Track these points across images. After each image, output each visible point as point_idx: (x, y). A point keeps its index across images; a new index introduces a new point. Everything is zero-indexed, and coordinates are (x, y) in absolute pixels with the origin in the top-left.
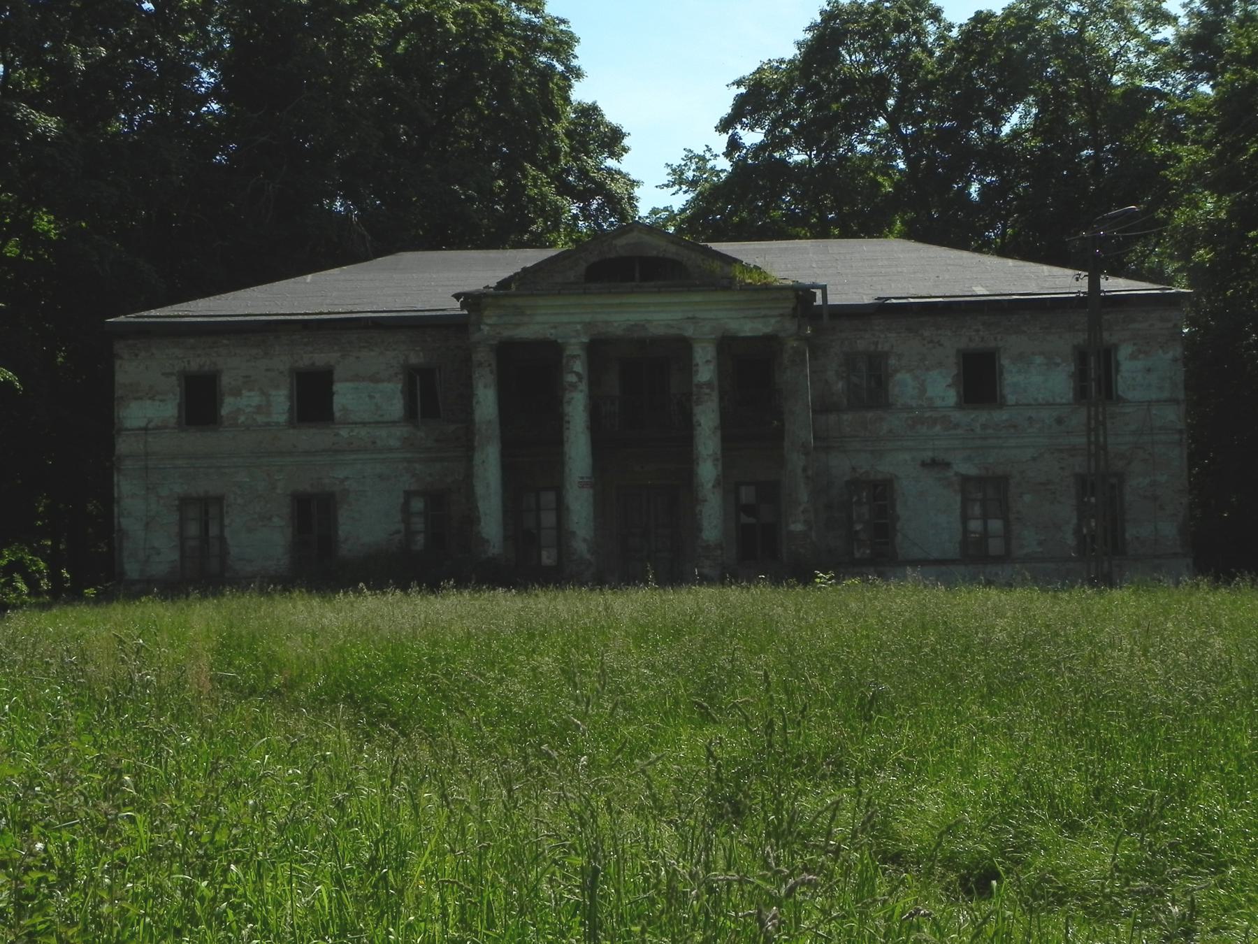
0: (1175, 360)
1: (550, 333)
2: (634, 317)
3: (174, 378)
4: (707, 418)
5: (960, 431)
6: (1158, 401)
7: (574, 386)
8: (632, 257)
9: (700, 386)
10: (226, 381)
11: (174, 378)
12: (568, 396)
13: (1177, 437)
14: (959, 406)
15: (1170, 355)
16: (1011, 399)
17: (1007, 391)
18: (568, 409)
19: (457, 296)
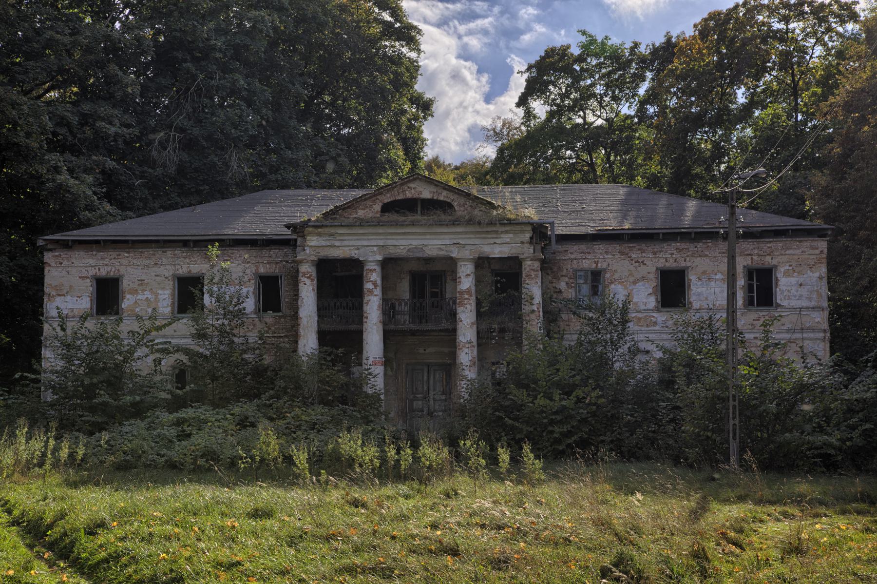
0: (821, 278)
1: (354, 254)
2: (416, 242)
3: (88, 280)
4: (467, 316)
5: (657, 328)
6: (807, 308)
7: (371, 292)
8: (437, 201)
9: (461, 293)
10: (125, 284)
11: (88, 280)
12: (366, 299)
13: (822, 335)
14: (657, 309)
15: (817, 274)
16: (696, 305)
17: (693, 298)
18: (367, 308)
19: (288, 226)
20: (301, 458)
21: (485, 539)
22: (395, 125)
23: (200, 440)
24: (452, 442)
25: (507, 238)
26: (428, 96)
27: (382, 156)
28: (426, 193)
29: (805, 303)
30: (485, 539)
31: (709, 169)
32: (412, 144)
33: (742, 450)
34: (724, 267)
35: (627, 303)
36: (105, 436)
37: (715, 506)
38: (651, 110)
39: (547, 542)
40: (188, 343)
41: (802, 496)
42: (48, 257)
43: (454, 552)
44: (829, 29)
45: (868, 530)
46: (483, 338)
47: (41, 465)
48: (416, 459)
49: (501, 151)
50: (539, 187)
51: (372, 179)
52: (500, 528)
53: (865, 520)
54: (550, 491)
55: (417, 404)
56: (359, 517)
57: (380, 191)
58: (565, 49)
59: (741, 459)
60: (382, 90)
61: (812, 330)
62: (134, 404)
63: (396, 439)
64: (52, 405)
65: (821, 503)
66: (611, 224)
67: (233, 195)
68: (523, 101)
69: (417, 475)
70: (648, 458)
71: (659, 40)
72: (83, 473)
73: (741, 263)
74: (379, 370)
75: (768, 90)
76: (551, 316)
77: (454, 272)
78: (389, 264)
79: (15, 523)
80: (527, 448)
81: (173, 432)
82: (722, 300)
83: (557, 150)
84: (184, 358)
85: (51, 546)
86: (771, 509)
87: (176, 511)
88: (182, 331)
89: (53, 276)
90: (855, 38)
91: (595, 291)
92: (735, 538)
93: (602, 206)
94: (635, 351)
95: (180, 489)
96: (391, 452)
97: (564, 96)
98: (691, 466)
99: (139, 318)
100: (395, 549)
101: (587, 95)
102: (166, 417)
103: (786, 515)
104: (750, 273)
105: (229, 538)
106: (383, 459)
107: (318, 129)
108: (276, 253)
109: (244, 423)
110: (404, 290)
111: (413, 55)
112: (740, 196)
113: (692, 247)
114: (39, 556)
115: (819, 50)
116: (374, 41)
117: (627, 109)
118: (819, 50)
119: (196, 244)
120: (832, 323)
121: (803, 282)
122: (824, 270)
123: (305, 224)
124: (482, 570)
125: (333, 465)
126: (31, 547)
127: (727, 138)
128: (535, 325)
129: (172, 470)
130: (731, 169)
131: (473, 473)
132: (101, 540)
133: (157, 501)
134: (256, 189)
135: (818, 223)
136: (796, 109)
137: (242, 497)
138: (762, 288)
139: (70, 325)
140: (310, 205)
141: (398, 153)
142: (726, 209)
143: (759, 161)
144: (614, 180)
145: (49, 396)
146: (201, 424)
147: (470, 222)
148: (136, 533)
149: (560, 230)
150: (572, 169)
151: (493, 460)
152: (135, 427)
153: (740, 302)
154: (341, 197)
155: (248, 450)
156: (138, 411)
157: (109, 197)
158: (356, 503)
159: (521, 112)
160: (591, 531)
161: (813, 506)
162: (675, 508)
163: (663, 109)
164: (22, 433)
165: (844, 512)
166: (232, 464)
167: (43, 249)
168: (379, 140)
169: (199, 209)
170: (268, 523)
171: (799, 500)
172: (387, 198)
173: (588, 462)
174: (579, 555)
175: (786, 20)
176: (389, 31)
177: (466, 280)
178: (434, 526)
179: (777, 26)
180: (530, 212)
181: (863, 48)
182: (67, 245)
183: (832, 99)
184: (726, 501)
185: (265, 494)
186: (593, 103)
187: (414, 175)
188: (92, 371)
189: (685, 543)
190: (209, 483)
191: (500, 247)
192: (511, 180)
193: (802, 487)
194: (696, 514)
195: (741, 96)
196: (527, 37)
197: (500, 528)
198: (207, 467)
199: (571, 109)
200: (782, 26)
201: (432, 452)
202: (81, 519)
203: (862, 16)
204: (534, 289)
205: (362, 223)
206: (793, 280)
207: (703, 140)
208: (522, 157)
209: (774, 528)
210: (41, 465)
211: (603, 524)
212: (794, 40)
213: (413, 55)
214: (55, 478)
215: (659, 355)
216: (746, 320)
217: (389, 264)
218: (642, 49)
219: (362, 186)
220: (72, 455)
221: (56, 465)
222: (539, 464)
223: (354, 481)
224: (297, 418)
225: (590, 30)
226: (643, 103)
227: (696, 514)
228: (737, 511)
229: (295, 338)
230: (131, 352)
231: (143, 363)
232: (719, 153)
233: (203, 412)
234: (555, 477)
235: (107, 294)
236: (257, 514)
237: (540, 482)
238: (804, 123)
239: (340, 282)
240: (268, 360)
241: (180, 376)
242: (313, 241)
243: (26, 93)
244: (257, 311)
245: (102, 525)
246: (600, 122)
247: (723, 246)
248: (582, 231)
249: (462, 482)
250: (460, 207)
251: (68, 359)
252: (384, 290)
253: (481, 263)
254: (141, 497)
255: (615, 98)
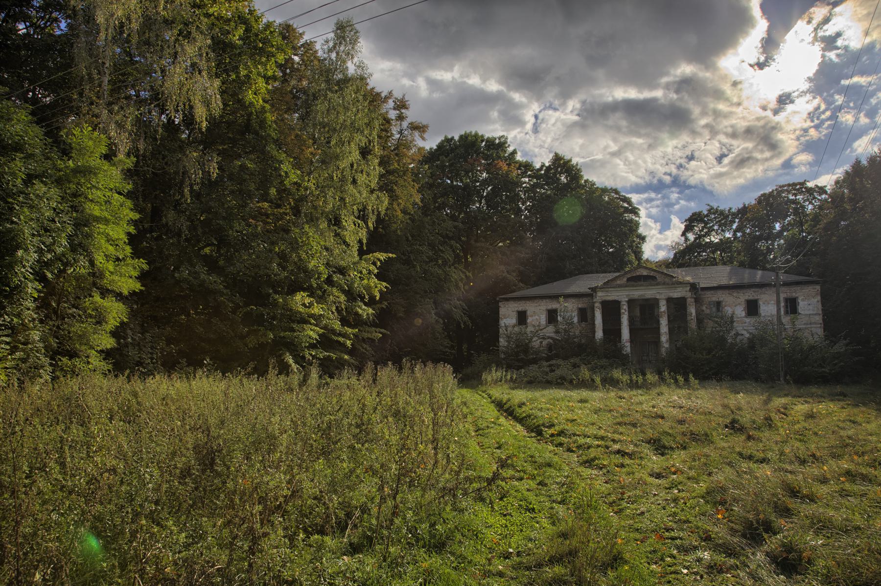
1: (616, 298)
10: (528, 313)
14: (746, 317)
16: (763, 314)
20: (598, 380)
21: (675, 412)
22: (631, 247)
23: (558, 372)
24: (660, 373)
25: (679, 289)
26: (644, 234)
27: (626, 259)
28: (645, 273)
29: (811, 312)
30: (675, 412)
31: (765, 258)
32: (638, 253)
33: (785, 375)
34: (775, 298)
35: (733, 313)
36: (523, 371)
37: (774, 398)
38: (739, 234)
39: (701, 414)
40: (553, 335)
41: (813, 394)
42: (500, 304)
43: (662, 417)
44: (814, 198)
45: (843, 408)
46: (671, 331)
47: (501, 381)
48: (645, 380)
49: (675, 254)
50: (692, 268)
51: (622, 269)
52: (681, 407)
53: (842, 403)
54: (702, 392)
55: (645, 358)
56: (623, 403)
57: (626, 273)
58: (700, 213)
59: (785, 380)
60: (625, 234)
61: (815, 323)
62: (533, 359)
63: (636, 372)
64: (504, 359)
65: (822, 396)
66: (724, 281)
67: (567, 278)
68: (684, 234)
69: (645, 386)
70: (745, 379)
71: (741, 206)
72: (516, 384)
73: (782, 296)
74: (628, 344)
75: (789, 224)
76: (700, 321)
77: (658, 304)
78: (631, 302)
79: (493, 402)
80: (691, 376)
81: (548, 369)
82: (775, 312)
83: (699, 253)
84: (551, 341)
85: (506, 411)
86: (800, 399)
87: (551, 399)
88: (550, 331)
89: (503, 311)
90: (826, 200)
91: (718, 310)
92: (784, 411)
93: (721, 275)
94: (737, 334)
95: (551, 391)
96: (634, 377)
97: (700, 231)
98: (763, 382)
99: (534, 326)
100: (638, 416)
101: (711, 230)
102: (545, 363)
103: (806, 402)
104: (787, 300)
105: (571, 410)
106: (631, 380)
107: (600, 250)
108: (585, 299)
109: (575, 366)
110: (637, 312)
111: (637, 219)
112: (780, 268)
113: (760, 291)
114: (502, 415)
115: (810, 207)
116: (621, 214)
117: (728, 235)
118: (810, 207)
119: (555, 297)
120: (824, 320)
121: (810, 304)
122: (819, 298)
123: (596, 287)
124: (674, 425)
125: (610, 383)
126: (499, 411)
127: (773, 245)
128: (693, 325)
129: (548, 384)
130: (775, 258)
131: (669, 385)
132: (523, 409)
133: (543, 396)
134: (577, 275)
135: (815, 279)
136: (802, 231)
137: (575, 394)
138: (792, 306)
139: (509, 329)
140: (598, 280)
141: (632, 257)
142: (774, 273)
143: (788, 254)
144: (724, 264)
145: (502, 356)
146: (558, 366)
147: (664, 284)
148: (536, 407)
149: (702, 286)
150: (705, 260)
151: (676, 381)
152: (534, 367)
153: (782, 313)
154: (610, 276)
155: (577, 377)
156: (535, 361)
157: (521, 281)
158: (621, 398)
159: (683, 238)
160: (720, 408)
161: (820, 398)
162: (757, 400)
163: (744, 234)
164: (494, 369)
165: (832, 400)
166: (571, 382)
167: (498, 302)
168: (625, 253)
169: (555, 283)
170: (586, 405)
171: (812, 395)
172: (629, 276)
173: (718, 381)
174: (716, 419)
175: (795, 195)
176: (627, 210)
177: (663, 308)
178: (654, 407)
179: (791, 197)
180: (689, 279)
181: (830, 205)
182: (507, 300)
183: (818, 227)
184: (779, 396)
185: (585, 393)
186: (713, 233)
187: (640, 266)
188: (517, 346)
189: (762, 414)
190: (562, 389)
191: (677, 293)
192: (680, 266)
193: (814, 389)
194: (766, 402)
195: (778, 226)
196: (677, 207)
197: (681, 407)
198: (561, 383)
199: (704, 236)
200: (793, 197)
201: (651, 377)
202: (516, 401)
203: (829, 192)
204: (692, 310)
205: (620, 286)
206: (806, 303)
207: (762, 245)
208: (684, 257)
209: (801, 408)
210: (501, 381)
211: (725, 406)
212: (799, 203)
213: (637, 219)
214: (506, 386)
215: (747, 335)
216: (786, 320)
217: (631, 302)
218: (733, 210)
219: (619, 271)
220: (511, 378)
221: (506, 381)
222: (697, 382)
223: (621, 389)
224: (595, 364)
225: (711, 204)
226: (735, 232)
227: (766, 402)
228: (783, 400)
229: (594, 332)
230: (531, 339)
231: (536, 343)
232: (769, 251)
233: (560, 362)
234: (704, 387)
235: (522, 317)
236: (582, 401)
237: (698, 389)
238: (806, 237)
239: (611, 310)
240: (583, 341)
241: (550, 347)
242: (600, 294)
243: (491, 245)
244: (578, 322)
245: (524, 404)
246: (717, 241)
247: (774, 289)
248: (712, 285)
249: (664, 389)
250: (660, 278)
251: (509, 342)
252: (629, 313)
253: (669, 300)
254: (537, 394)
255: (722, 230)
